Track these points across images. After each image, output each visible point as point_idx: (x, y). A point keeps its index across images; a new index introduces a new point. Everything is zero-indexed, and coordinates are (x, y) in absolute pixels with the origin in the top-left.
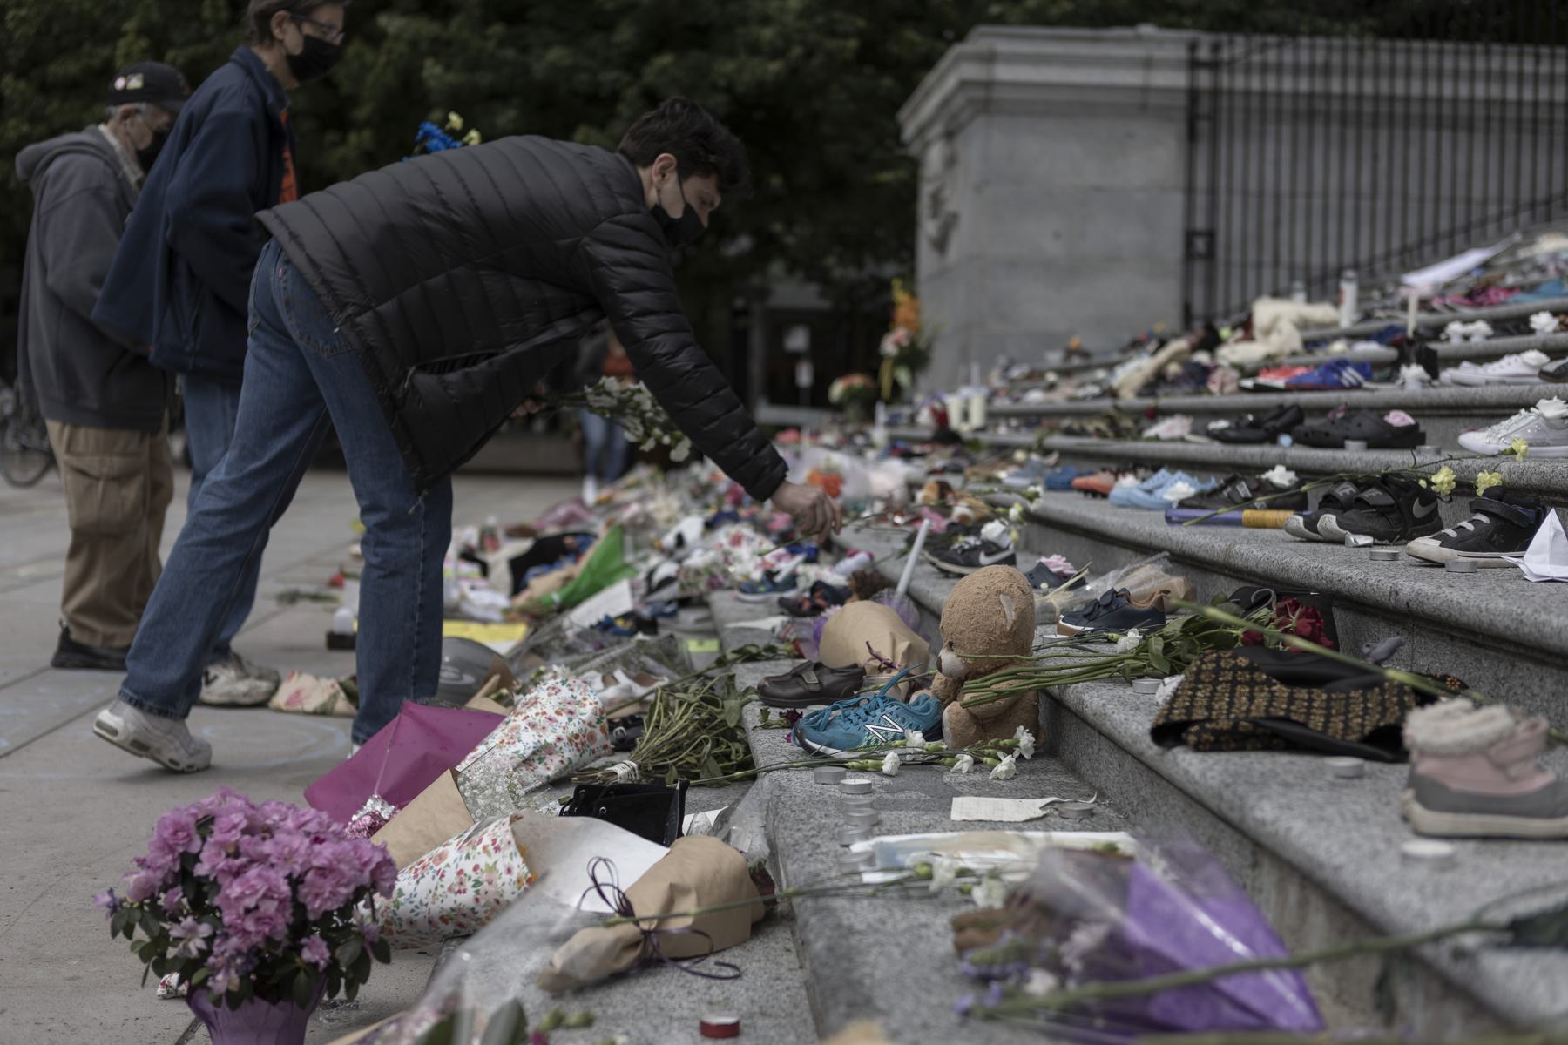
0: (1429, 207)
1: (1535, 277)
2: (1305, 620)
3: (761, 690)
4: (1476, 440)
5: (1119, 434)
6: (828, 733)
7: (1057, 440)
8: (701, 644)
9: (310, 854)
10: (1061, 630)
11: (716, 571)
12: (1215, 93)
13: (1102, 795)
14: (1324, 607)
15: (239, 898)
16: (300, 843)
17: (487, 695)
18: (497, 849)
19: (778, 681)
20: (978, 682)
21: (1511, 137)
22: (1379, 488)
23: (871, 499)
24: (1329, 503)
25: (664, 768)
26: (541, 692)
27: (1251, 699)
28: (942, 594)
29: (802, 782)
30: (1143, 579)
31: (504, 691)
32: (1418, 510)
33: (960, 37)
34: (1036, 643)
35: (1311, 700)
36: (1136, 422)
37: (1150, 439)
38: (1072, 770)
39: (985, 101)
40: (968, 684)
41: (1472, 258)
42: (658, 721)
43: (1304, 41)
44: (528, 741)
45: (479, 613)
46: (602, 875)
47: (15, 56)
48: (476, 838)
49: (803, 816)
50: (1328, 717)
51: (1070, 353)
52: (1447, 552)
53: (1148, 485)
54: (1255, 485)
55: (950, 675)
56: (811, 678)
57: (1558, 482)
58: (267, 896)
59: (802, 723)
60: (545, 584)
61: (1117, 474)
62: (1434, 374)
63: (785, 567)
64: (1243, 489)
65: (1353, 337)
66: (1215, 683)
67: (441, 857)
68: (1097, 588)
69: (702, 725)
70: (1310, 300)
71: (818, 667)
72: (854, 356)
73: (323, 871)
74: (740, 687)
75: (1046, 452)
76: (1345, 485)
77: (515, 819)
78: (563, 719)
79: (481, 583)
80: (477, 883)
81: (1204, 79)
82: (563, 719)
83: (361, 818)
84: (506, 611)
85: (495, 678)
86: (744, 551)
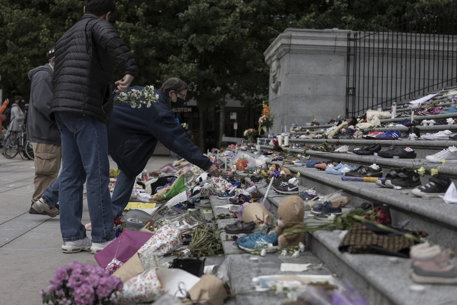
0: (417, 81)
1: (448, 103)
2: (382, 214)
3: (226, 229)
4: (430, 158)
5: (328, 150)
6: (246, 244)
7: (310, 151)
8: (207, 211)
9: (99, 281)
10: (312, 213)
11: (211, 190)
12: (355, 48)
13: (324, 263)
14: (387, 211)
15: (80, 293)
16: (97, 277)
17: (146, 228)
18: (152, 278)
19: (230, 226)
20: (288, 230)
21: (441, 61)
22: (403, 172)
23: (256, 168)
24: (389, 176)
25: (198, 251)
26: (162, 229)
27: (367, 238)
28: (277, 200)
29: (238, 258)
30: (335, 197)
31: (151, 227)
32: (414, 179)
33: (282, 31)
34: (305, 217)
35: (384, 239)
36: (333, 146)
37: (336, 152)
38: (315, 255)
39: (289, 50)
40: (285, 230)
41: (430, 96)
42: (196, 237)
43: (381, 33)
44: (159, 243)
45: (142, 200)
46: (182, 287)
47: (10, 34)
48: (145, 275)
49: (239, 269)
50: (389, 244)
51: (313, 123)
52: (423, 193)
53: (336, 168)
54: (367, 169)
55: (280, 227)
56: (240, 226)
57: (454, 172)
58: (88, 293)
59: (238, 240)
60: (161, 192)
61: (327, 163)
62: (419, 135)
63: (232, 189)
64: (364, 170)
65: (395, 122)
66: (356, 233)
67: (135, 280)
68: (323, 199)
69: (209, 239)
70: (384, 110)
71: (242, 222)
72: (251, 123)
73: (103, 286)
74: (219, 227)
75: (307, 155)
76: (393, 171)
77: (157, 269)
78: (169, 237)
79: (143, 190)
80: (146, 288)
81: (352, 44)
82: (169, 237)
83: (111, 265)
84: (150, 199)
85: (149, 223)
86: (219, 184)
